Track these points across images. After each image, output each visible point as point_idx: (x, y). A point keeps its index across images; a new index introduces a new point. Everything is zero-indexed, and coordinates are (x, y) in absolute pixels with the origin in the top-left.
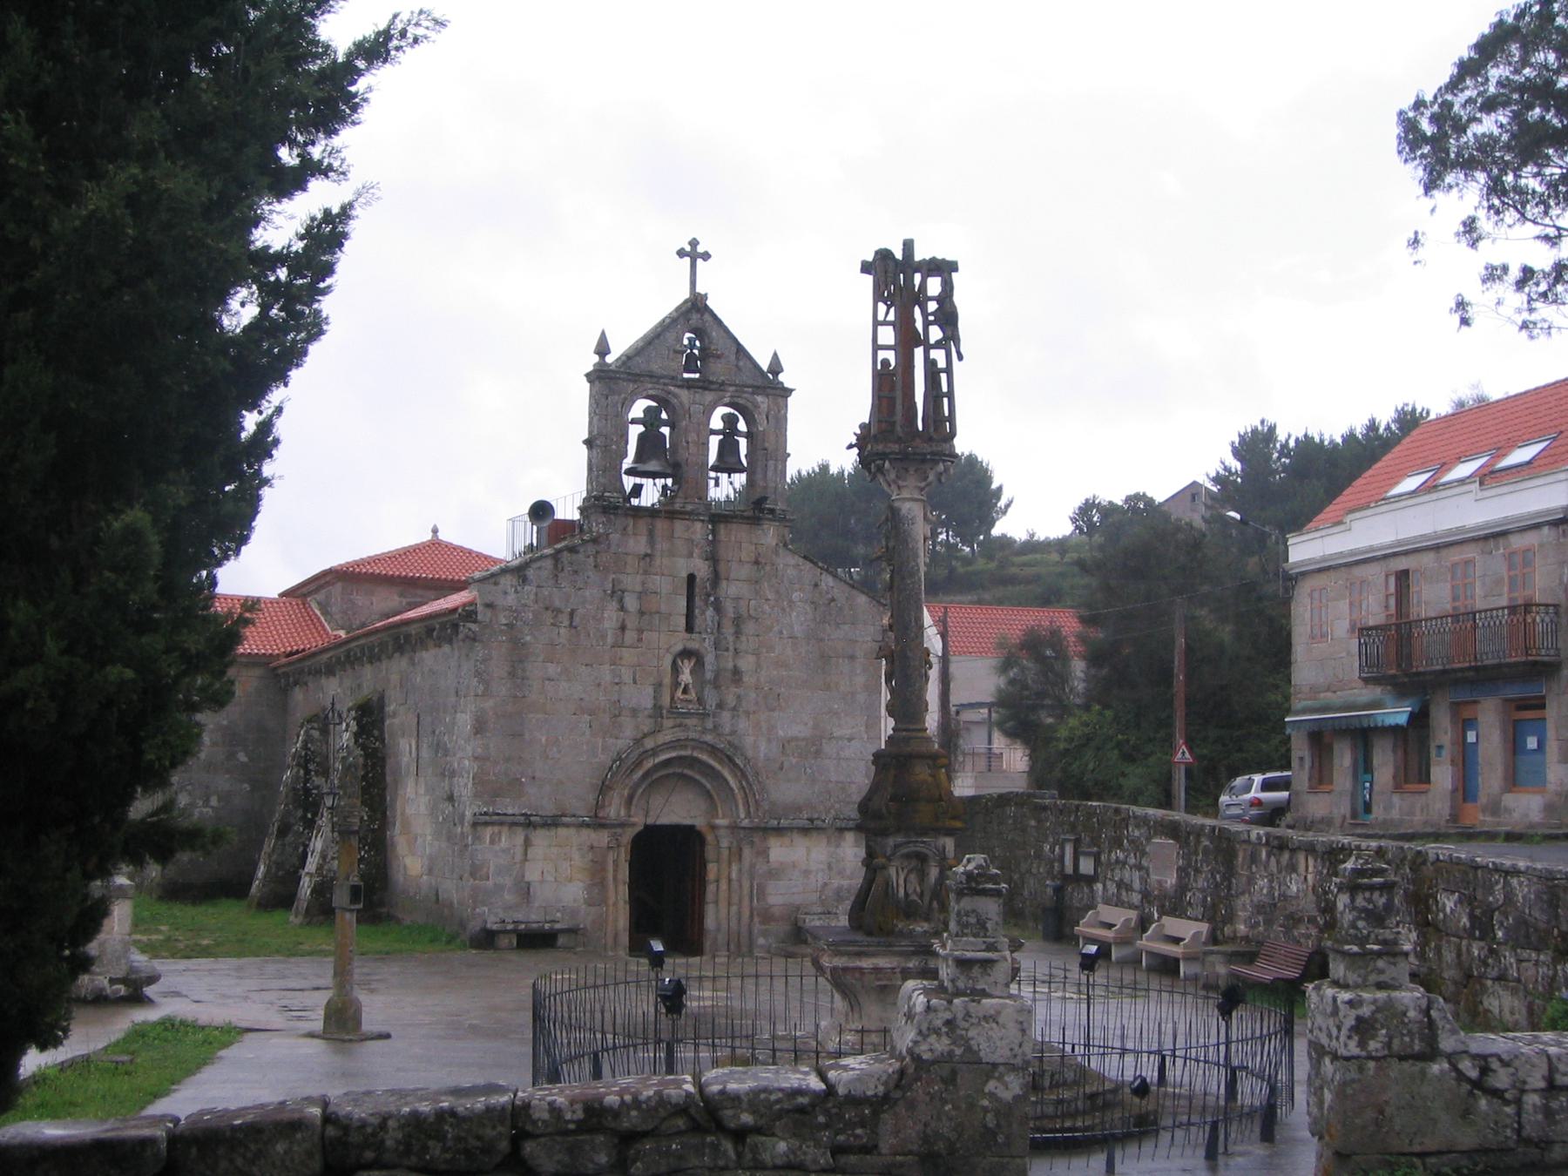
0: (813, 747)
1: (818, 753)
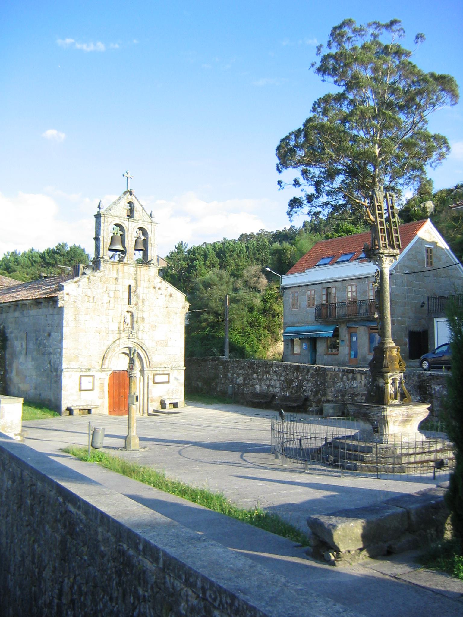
1: (166, 345)
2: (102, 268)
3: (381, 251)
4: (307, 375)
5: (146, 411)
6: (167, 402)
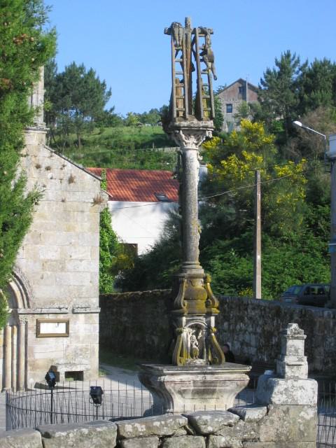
0: (61, 265)
1: (63, 269)
3: (177, 123)
5: (22, 385)
6: (62, 370)
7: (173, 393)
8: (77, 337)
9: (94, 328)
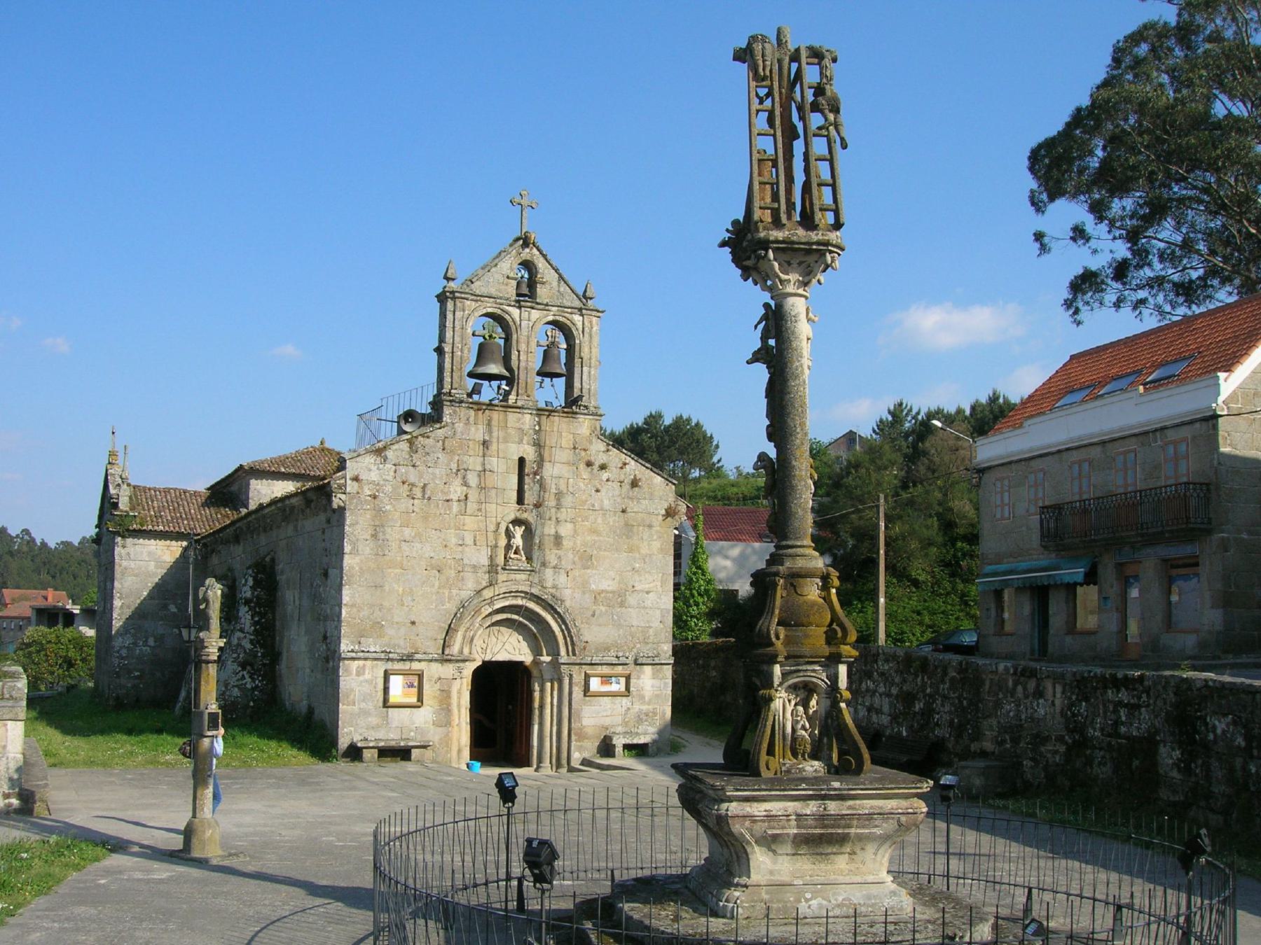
0: (619, 598)
1: (622, 605)
2: (446, 419)
4: (943, 682)
5: (564, 762)
6: (619, 742)
7: (748, 843)
8: (642, 697)
9: (666, 684)
